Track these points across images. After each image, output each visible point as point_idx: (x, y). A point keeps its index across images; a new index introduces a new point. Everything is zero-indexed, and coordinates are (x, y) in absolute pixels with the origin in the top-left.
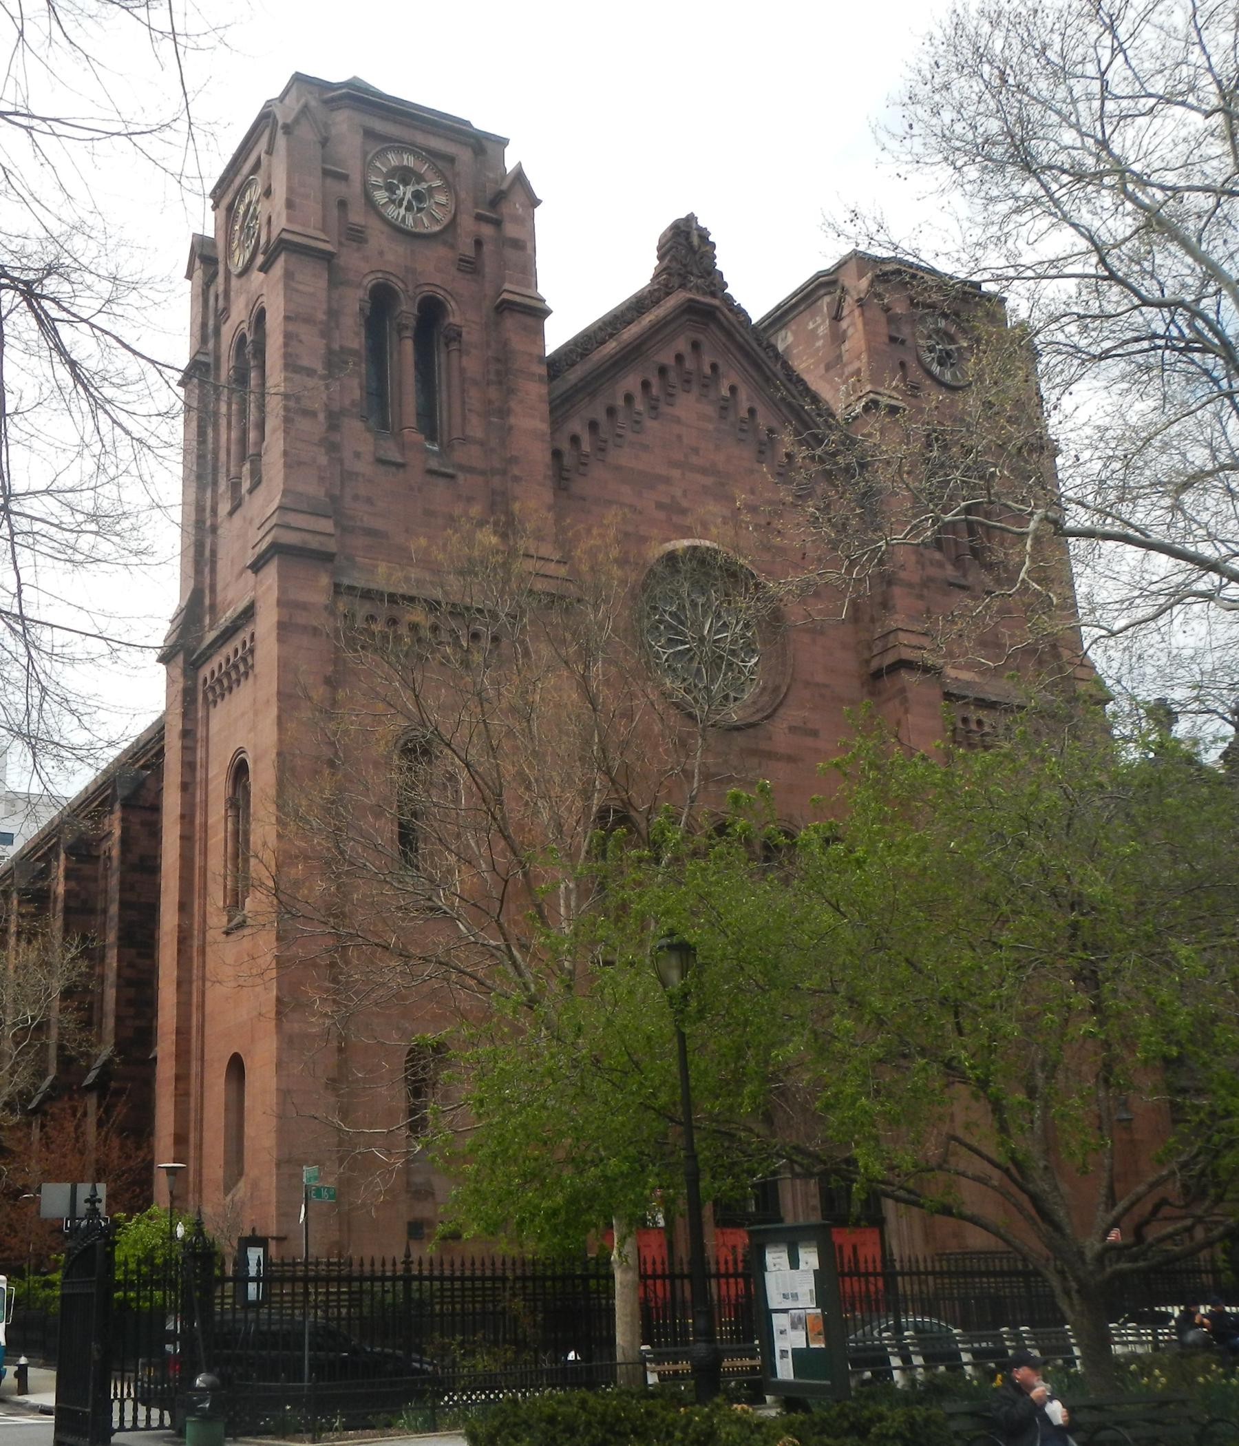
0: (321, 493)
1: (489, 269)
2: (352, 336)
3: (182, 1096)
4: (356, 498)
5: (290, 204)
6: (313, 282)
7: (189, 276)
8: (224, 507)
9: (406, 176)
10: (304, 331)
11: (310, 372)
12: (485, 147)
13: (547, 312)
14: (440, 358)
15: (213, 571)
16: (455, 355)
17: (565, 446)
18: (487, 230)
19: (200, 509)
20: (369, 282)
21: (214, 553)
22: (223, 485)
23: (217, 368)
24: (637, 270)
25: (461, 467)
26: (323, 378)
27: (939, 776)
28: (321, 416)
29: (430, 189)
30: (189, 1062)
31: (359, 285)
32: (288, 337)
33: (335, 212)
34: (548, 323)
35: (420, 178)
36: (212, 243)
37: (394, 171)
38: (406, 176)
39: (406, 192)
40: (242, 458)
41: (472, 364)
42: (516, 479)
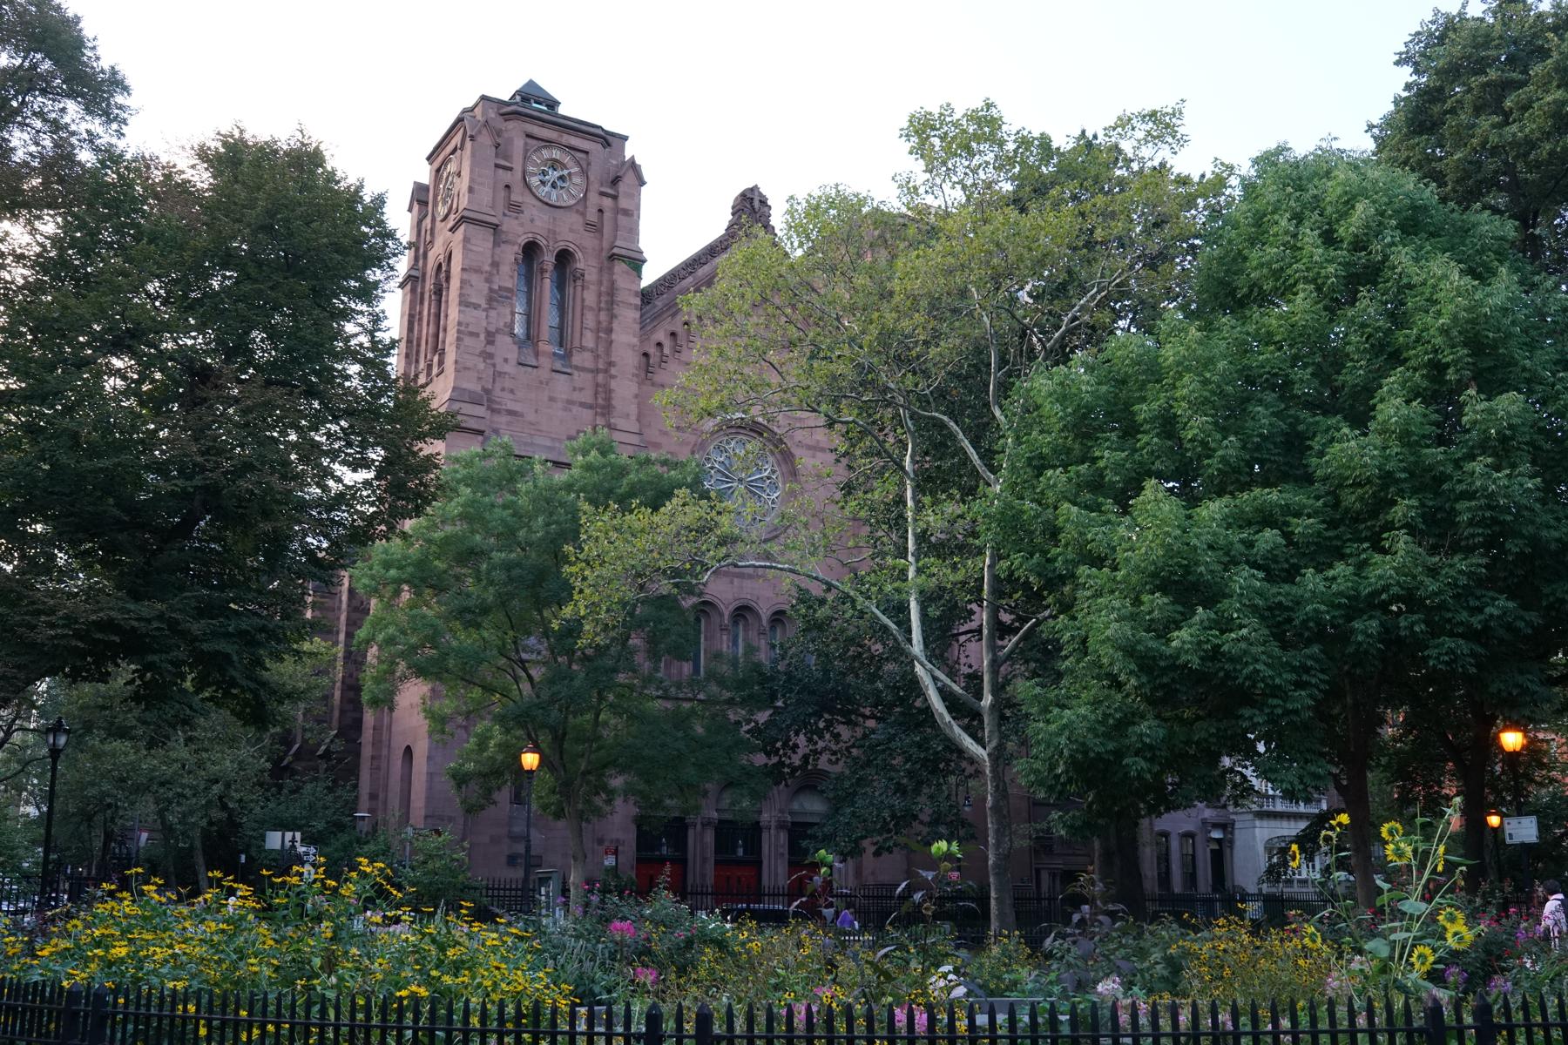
0: (478, 389)
1: (607, 229)
2: (508, 276)
3: (375, 769)
5: (471, 190)
7: (410, 210)
9: (555, 164)
10: (476, 280)
11: (476, 306)
12: (610, 141)
13: (644, 261)
14: (570, 290)
17: (652, 350)
18: (607, 203)
20: (522, 240)
22: (422, 365)
23: (424, 281)
24: (715, 224)
25: (577, 368)
27: (485, 634)
28: (482, 337)
31: (514, 244)
33: (502, 193)
34: (645, 268)
35: (564, 166)
37: (545, 162)
38: (555, 164)
39: (553, 175)
40: (435, 349)
41: (590, 297)
42: (613, 377)
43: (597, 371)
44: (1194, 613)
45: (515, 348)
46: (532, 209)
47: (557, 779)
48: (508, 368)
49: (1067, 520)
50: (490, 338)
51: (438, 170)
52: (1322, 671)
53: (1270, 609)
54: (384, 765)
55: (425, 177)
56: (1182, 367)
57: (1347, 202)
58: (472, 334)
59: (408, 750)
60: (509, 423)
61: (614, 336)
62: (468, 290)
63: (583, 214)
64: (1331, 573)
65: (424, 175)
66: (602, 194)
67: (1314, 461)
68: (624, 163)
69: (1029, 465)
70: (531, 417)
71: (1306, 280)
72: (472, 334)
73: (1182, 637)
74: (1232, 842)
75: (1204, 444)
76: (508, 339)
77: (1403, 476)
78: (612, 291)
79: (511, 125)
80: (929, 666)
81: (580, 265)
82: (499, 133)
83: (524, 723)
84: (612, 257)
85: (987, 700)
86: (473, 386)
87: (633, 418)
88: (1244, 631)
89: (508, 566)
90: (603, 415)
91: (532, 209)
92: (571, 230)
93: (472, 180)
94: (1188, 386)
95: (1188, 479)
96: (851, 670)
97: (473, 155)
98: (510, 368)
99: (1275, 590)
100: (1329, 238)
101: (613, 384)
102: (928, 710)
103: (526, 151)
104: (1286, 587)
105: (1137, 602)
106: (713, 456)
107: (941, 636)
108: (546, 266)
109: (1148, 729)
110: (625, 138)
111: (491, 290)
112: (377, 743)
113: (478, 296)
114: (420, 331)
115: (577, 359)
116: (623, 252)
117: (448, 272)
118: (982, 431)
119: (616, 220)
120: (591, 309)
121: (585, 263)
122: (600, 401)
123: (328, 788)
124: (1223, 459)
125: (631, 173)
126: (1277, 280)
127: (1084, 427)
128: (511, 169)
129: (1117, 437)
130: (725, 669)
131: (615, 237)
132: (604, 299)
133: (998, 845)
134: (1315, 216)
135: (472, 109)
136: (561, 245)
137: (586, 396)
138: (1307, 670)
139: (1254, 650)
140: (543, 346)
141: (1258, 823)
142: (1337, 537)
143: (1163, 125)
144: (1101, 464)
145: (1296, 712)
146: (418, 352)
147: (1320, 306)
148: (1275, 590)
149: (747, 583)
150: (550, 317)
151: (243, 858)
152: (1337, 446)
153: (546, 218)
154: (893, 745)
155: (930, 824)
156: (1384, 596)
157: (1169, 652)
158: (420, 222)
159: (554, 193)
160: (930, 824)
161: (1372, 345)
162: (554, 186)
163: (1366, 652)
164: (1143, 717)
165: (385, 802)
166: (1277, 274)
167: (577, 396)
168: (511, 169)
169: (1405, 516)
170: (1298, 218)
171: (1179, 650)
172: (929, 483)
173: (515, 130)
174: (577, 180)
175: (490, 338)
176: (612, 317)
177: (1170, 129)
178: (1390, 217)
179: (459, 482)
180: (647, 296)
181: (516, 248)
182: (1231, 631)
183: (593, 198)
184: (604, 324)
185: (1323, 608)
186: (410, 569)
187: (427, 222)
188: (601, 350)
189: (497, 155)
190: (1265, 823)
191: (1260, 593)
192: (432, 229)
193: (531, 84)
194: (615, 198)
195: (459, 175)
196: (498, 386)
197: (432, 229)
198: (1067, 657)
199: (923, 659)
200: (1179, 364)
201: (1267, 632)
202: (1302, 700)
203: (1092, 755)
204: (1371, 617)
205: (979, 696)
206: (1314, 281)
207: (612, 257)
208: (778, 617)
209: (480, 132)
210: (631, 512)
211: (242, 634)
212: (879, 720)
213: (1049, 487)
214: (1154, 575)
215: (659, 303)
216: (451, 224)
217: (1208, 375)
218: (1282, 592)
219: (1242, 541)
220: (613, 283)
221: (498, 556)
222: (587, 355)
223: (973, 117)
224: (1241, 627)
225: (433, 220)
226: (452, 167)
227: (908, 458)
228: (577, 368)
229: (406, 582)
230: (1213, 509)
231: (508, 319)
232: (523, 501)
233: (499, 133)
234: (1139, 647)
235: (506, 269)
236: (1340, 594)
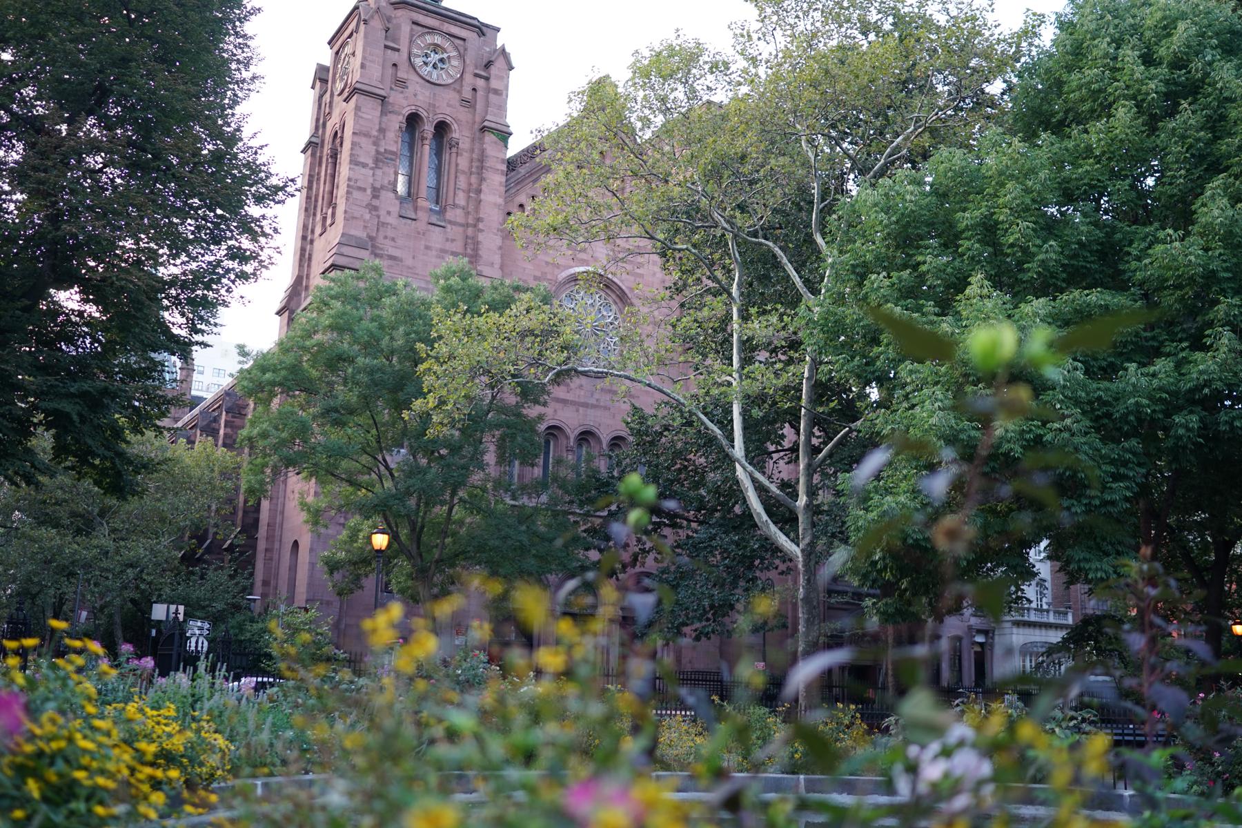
2: (393, 141)
3: (268, 560)
4: (386, 237)
5: (363, 66)
6: (372, 110)
7: (313, 87)
8: (318, 230)
9: (436, 48)
10: (364, 141)
11: (364, 165)
12: (482, 30)
14: (446, 157)
15: (309, 266)
16: (454, 155)
18: (480, 83)
19: (305, 227)
21: (310, 255)
22: (319, 217)
23: (322, 146)
25: (450, 222)
26: (372, 169)
27: (349, 431)
28: (369, 191)
29: (449, 57)
30: (273, 542)
31: (399, 114)
32: (353, 144)
33: (390, 71)
34: (511, 140)
36: (327, 69)
38: (436, 48)
39: (434, 58)
41: (463, 162)
43: (467, 225)
45: (397, 202)
47: (413, 566)
48: (390, 220)
51: (337, 53)
52: (1139, 465)
53: (1090, 403)
54: (276, 557)
55: (327, 60)
56: (1003, 176)
57: (1165, 28)
58: (360, 189)
59: (296, 544)
60: (390, 267)
61: (482, 196)
62: (357, 151)
63: (459, 92)
64: (1152, 369)
65: (326, 58)
66: (476, 75)
67: (1134, 264)
68: (495, 50)
69: (853, 272)
70: (409, 262)
71: (1126, 97)
72: (360, 189)
74: (992, 646)
75: (1025, 250)
76: (392, 195)
77: (1226, 275)
78: (482, 159)
79: (400, 13)
80: (750, 468)
81: (455, 135)
82: (389, 19)
83: (384, 511)
84: (483, 129)
85: (802, 500)
86: (360, 233)
87: (497, 266)
88: (1068, 421)
89: (371, 371)
92: (449, 105)
93: (364, 58)
94: (1012, 192)
96: (678, 481)
97: (366, 36)
98: (392, 220)
99: (1095, 386)
100: (1148, 60)
101: (481, 237)
102: (748, 515)
103: (412, 36)
104: (1106, 384)
106: (565, 303)
107: (761, 437)
108: (426, 134)
110: (498, 30)
111: (378, 152)
112: (270, 538)
113: (367, 153)
114: (318, 189)
115: (450, 215)
116: (493, 125)
117: (342, 138)
118: (806, 255)
119: (487, 98)
120: (463, 172)
121: (459, 133)
122: (469, 251)
123: (230, 576)
125: (501, 59)
126: (1094, 101)
127: (907, 236)
128: (398, 50)
129: (940, 247)
130: (563, 472)
131: (486, 113)
133: (807, 634)
134: (1134, 40)
136: (440, 117)
137: (458, 246)
138: (1125, 463)
139: (1076, 440)
140: (421, 203)
141: (1015, 630)
142: (1153, 338)
145: (1113, 503)
146: (315, 207)
147: (1140, 120)
148: (1095, 386)
149: (590, 412)
150: (427, 179)
151: (154, 632)
152: (1159, 248)
153: (427, 94)
154: (714, 543)
156: (1206, 391)
158: (321, 97)
159: (435, 73)
161: (1193, 156)
163: (1184, 448)
166: (1095, 94)
167: (449, 246)
168: (398, 50)
169: (1227, 314)
170: (1118, 43)
172: (754, 302)
174: (455, 63)
176: (482, 180)
178: (1211, 38)
179: (332, 297)
180: (512, 164)
183: (469, 78)
184: (475, 186)
185: (1145, 401)
186: (283, 373)
187: (327, 97)
188: (471, 208)
190: (1021, 630)
191: (1084, 387)
192: (331, 103)
194: (487, 79)
195: (353, 54)
196: (381, 235)
197: (331, 103)
200: (1001, 173)
201: (1088, 423)
202: (1121, 490)
204: (1191, 412)
205: (795, 496)
206: (1134, 98)
207: (483, 129)
208: (617, 441)
209: (372, 17)
210: (480, 315)
211: (83, 395)
212: (701, 523)
213: (873, 290)
215: (522, 170)
216: (346, 94)
217: (1030, 183)
218: (1100, 389)
220: (483, 151)
221: (361, 361)
222: (459, 212)
225: (332, 95)
226: (348, 50)
227: (735, 286)
228: (450, 222)
229: (280, 384)
232: (386, 314)
233: (389, 19)
235: (391, 135)
236: (1161, 389)
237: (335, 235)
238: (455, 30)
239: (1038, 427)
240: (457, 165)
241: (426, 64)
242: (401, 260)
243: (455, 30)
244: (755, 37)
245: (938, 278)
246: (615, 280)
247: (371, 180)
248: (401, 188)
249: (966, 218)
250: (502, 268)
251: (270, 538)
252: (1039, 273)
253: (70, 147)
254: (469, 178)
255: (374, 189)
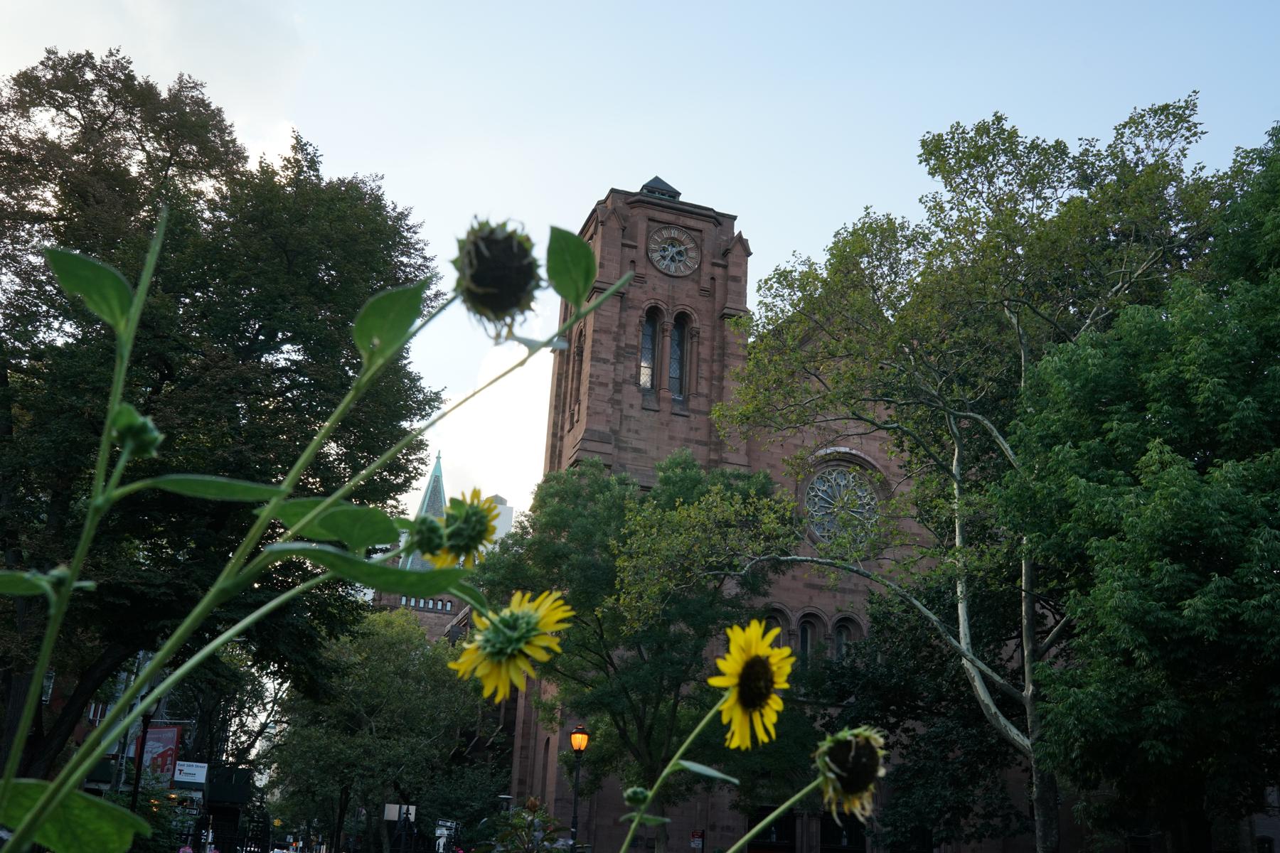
1: (718, 295)
2: (633, 336)
8: (567, 427)
9: (673, 242)
11: (605, 361)
12: (723, 221)
14: (688, 346)
18: (718, 271)
20: (646, 305)
21: (561, 452)
25: (694, 411)
28: (611, 386)
32: (594, 341)
35: (681, 243)
38: (673, 242)
39: (672, 251)
41: (704, 351)
44: (1209, 580)
45: (640, 395)
46: (653, 279)
49: (1075, 494)
50: (618, 387)
56: (1190, 328)
58: (601, 384)
61: (725, 383)
63: (698, 282)
66: (714, 264)
68: (733, 238)
70: (653, 453)
72: (601, 384)
73: (1193, 606)
75: (1218, 407)
76: (634, 388)
79: (635, 211)
81: (696, 325)
85: (1029, 690)
86: (602, 427)
87: (742, 452)
88: (1267, 597)
90: (716, 451)
91: (653, 279)
92: (688, 296)
94: (1198, 346)
95: (1200, 442)
97: (603, 237)
98: (635, 413)
103: (648, 232)
105: (1147, 572)
106: (817, 486)
109: (1164, 708)
110: (734, 218)
111: (618, 347)
112: (526, 735)
114: (566, 387)
115: (693, 404)
119: (726, 285)
120: (705, 360)
124: (1240, 422)
128: (635, 247)
132: (716, 352)
135: (605, 201)
143: (1176, 118)
144: (1111, 436)
149: (849, 598)
155: (984, 817)
157: (1182, 623)
160: (984, 817)
162: (673, 259)
164: (1162, 697)
165: (532, 787)
167: (693, 435)
168: (635, 247)
171: (1194, 621)
173: (639, 215)
175: (618, 387)
176: (724, 367)
177: (1182, 119)
181: (640, 312)
182: (1253, 598)
183: (707, 268)
189: (623, 237)
193: (657, 180)
198: (1078, 635)
199: (971, 656)
200: (1187, 327)
203: (1104, 737)
205: (1022, 688)
209: (609, 218)
214: (1163, 540)
217: (1218, 336)
219: (1264, 505)
220: (723, 338)
222: (702, 400)
223: (982, 129)
224: (1262, 592)
228: (694, 411)
230: (1227, 471)
231: (634, 372)
232: (599, 508)
233: (626, 219)
234: (1148, 618)
235: (631, 330)
237: (579, 431)
238: (691, 223)
239: (1235, 605)
240: (698, 354)
241: (664, 258)
242: (646, 452)
243: (691, 223)
244: (947, 206)
245: (1128, 446)
246: (869, 459)
247: (612, 376)
248: (645, 378)
249: (1152, 378)
250: (748, 454)
251: (526, 735)
252: (1236, 433)
253: (221, 379)
254: (711, 367)
255: (616, 383)
